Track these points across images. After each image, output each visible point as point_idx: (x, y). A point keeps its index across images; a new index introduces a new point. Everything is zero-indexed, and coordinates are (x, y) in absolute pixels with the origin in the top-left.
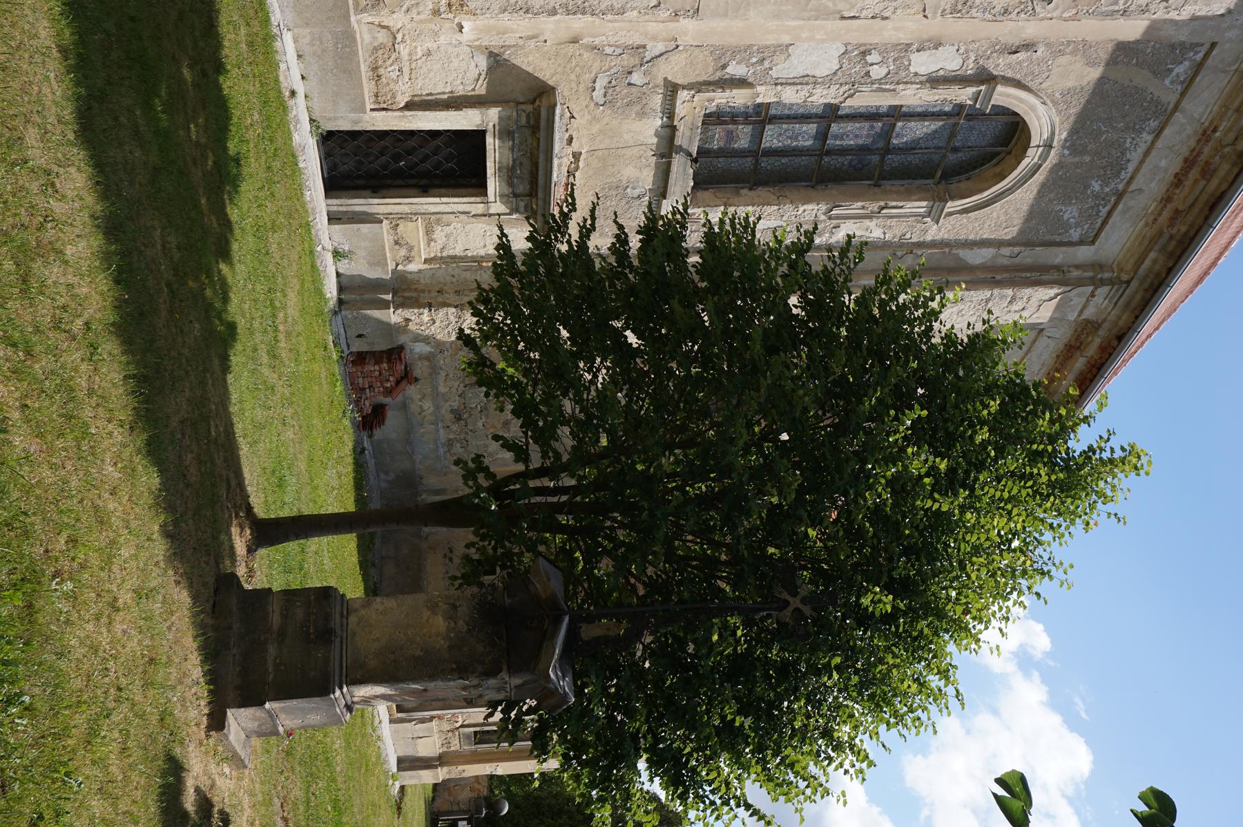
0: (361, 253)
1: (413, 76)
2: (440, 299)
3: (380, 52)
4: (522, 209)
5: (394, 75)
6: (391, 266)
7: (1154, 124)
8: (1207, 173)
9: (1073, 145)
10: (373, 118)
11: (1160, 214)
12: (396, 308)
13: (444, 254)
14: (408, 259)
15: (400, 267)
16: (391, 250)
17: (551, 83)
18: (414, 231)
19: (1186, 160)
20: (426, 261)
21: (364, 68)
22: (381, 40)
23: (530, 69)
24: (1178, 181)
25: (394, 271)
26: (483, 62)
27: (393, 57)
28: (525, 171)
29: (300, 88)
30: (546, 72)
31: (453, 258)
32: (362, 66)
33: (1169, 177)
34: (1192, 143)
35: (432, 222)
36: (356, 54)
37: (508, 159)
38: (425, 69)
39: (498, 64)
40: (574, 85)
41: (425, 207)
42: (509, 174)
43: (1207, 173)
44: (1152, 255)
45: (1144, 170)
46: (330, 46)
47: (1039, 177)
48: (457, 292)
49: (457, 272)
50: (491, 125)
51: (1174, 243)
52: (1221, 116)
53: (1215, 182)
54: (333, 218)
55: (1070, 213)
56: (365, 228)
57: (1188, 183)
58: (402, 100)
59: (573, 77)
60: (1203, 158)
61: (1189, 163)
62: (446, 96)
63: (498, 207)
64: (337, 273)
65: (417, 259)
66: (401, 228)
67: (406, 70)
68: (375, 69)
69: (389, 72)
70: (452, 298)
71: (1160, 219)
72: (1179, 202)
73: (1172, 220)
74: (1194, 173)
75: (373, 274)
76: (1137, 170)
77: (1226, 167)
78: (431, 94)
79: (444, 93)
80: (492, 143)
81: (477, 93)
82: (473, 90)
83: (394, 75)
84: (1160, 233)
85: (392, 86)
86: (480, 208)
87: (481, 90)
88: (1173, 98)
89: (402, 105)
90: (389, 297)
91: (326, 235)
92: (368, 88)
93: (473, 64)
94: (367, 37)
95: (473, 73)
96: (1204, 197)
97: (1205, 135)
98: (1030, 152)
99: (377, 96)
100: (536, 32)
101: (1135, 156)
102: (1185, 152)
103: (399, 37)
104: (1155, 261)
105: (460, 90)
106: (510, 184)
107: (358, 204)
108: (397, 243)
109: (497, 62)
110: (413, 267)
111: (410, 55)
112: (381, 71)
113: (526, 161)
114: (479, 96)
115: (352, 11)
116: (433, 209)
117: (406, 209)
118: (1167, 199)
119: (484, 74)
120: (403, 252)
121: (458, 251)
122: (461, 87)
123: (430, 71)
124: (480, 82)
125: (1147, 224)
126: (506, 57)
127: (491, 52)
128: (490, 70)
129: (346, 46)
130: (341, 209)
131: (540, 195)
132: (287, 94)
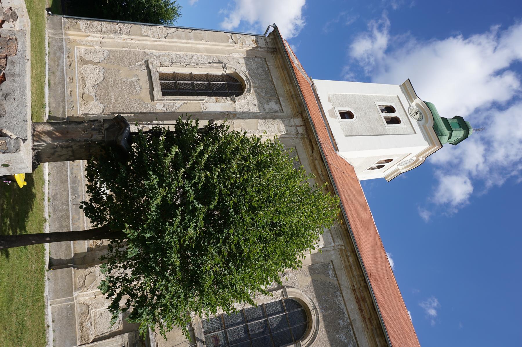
3: (84, 316)
5: (88, 326)
7: (338, 293)
8: (364, 300)
9: (322, 307)
11: (367, 325)
19: (357, 302)
21: (77, 324)
22: (84, 310)
24: (361, 310)
27: (88, 317)
29: (50, 324)
33: (359, 312)
34: (354, 296)
36: (75, 316)
38: (100, 322)
43: (364, 300)
44: (377, 340)
45: (349, 311)
46: (65, 314)
47: (322, 324)
50: (126, 344)
51: (378, 330)
52: (352, 282)
53: (368, 302)
55: (343, 337)
57: (363, 308)
58: (92, 338)
60: (359, 297)
61: (358, 302)
62: (108, 334)
67: (93, 324)
68: (81, 324)
69: (86, 325)
71: (368, 326)
72: (367, 317)
73: (371, 323)
74: (362, 304)
76: (348, 312)
77: (365, 293)
78: (102, 334)
83: (88, 326)
84: (372, 330)
85: (87, 331)
88: (336, 282)
92: (78, 334)
96: (370, 306)
97: (354, 290)
98: (312, 312)
101: (343, 306)
102: (355, 300)
103: (90, 307)
104: (380, 342)
111: (95, 317)
115: (74, 290)
118: (364, 318)
125: (367, 332)
129: (71, 314)
132: (46, 325)
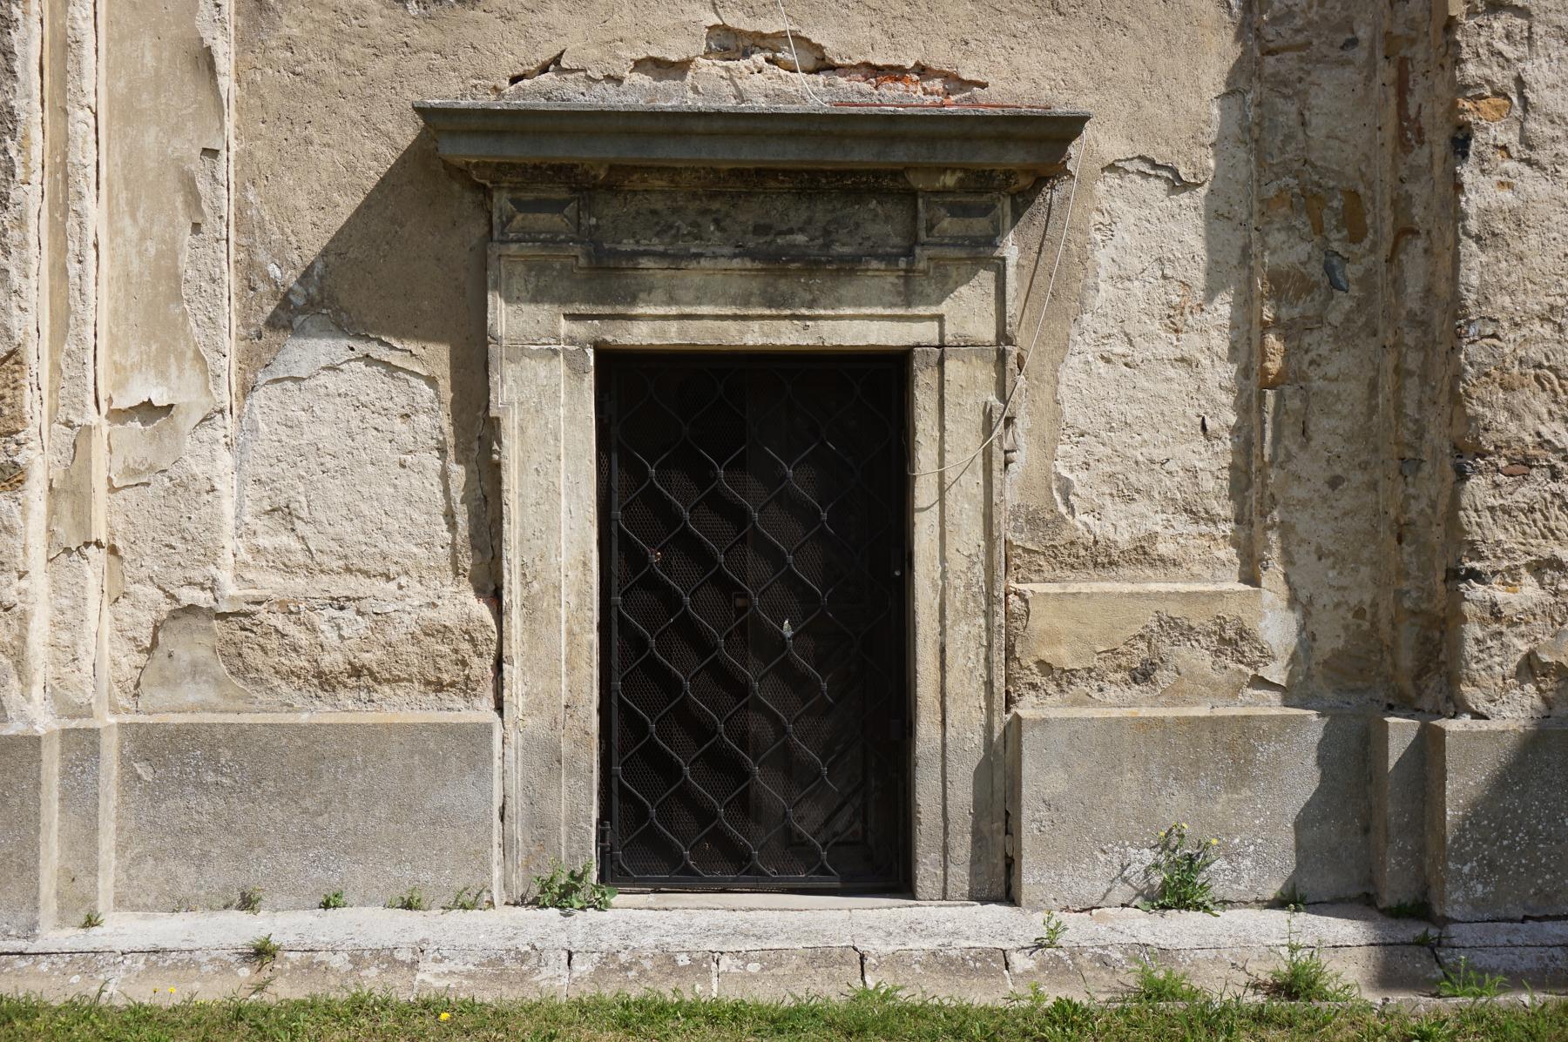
0: (1176, 807)
1: (376, 566)
2: (1436, 534)
3: (255, 658)
4: (979, 225)
6: (1271, 706)
10: (535, 707)
12: (1459, 707)
13: (1224, 509)
14: (1234, 640)
15: (1276, 672)
16: (1176, 696)
17: (407, 133)
18: (1068, 613)
20: (1251, 578)
23: (347, 205)
25: (1290, 694)
26: (312, 352)
27: (278, 621)
28: (799, 215)
30: (376, 145)
31: (1242, 479)
32: (304, 718)
35: (1035, 541)
36: (243, 730)
37: (736, 272)
38: (347, 529)
39: (331, 297)
40: (416, 63)
41: (957, 563)
42: (790, 270)
48: (1409, 465)
49: (1312, 468)
54: (1000, 883)
56: (1040, 780)
59: (382, 67)
63: (968, 310)
64: (1279, 903)
65: (1231, 610)
66: (1062, 656)
68: (325, 681)
69: (339, 636)
70: (1429, 486)
75: (1301, 780)
78: (450, 516)
79: (444, 476)
80: (649, 328)
81: (443, 371)
82: (432, 381)
85: (394, 635)
86: (968, 381)
87: (436, 357)
89: (482, 610)
90: (1401, 731)
91: (1084, 924)
93: (326, 379)
94: (191, 693)
95: (361, 380)
99: (439, 686)
100: (171, 181)
103: (188, 596)
105: (436, 421)
106: (849, 267)
107: (942, 790)
108: (1143, 675)
109: (312, 305)
110: (1276, 626)
112: (332, 661)
113: (748, 214)
114: (457, 365)
116: (968, 537)
117: (966, 637)
119: (361, 347)
120: (1197, 657)
121: (1211, 464)
122: (423, 420)
123: (353, 515)
124: (396, 359)
126: (291, 278)
127: (272, 323)
128: (347, 324)
130: (962, 847)
131: (899, 155)
